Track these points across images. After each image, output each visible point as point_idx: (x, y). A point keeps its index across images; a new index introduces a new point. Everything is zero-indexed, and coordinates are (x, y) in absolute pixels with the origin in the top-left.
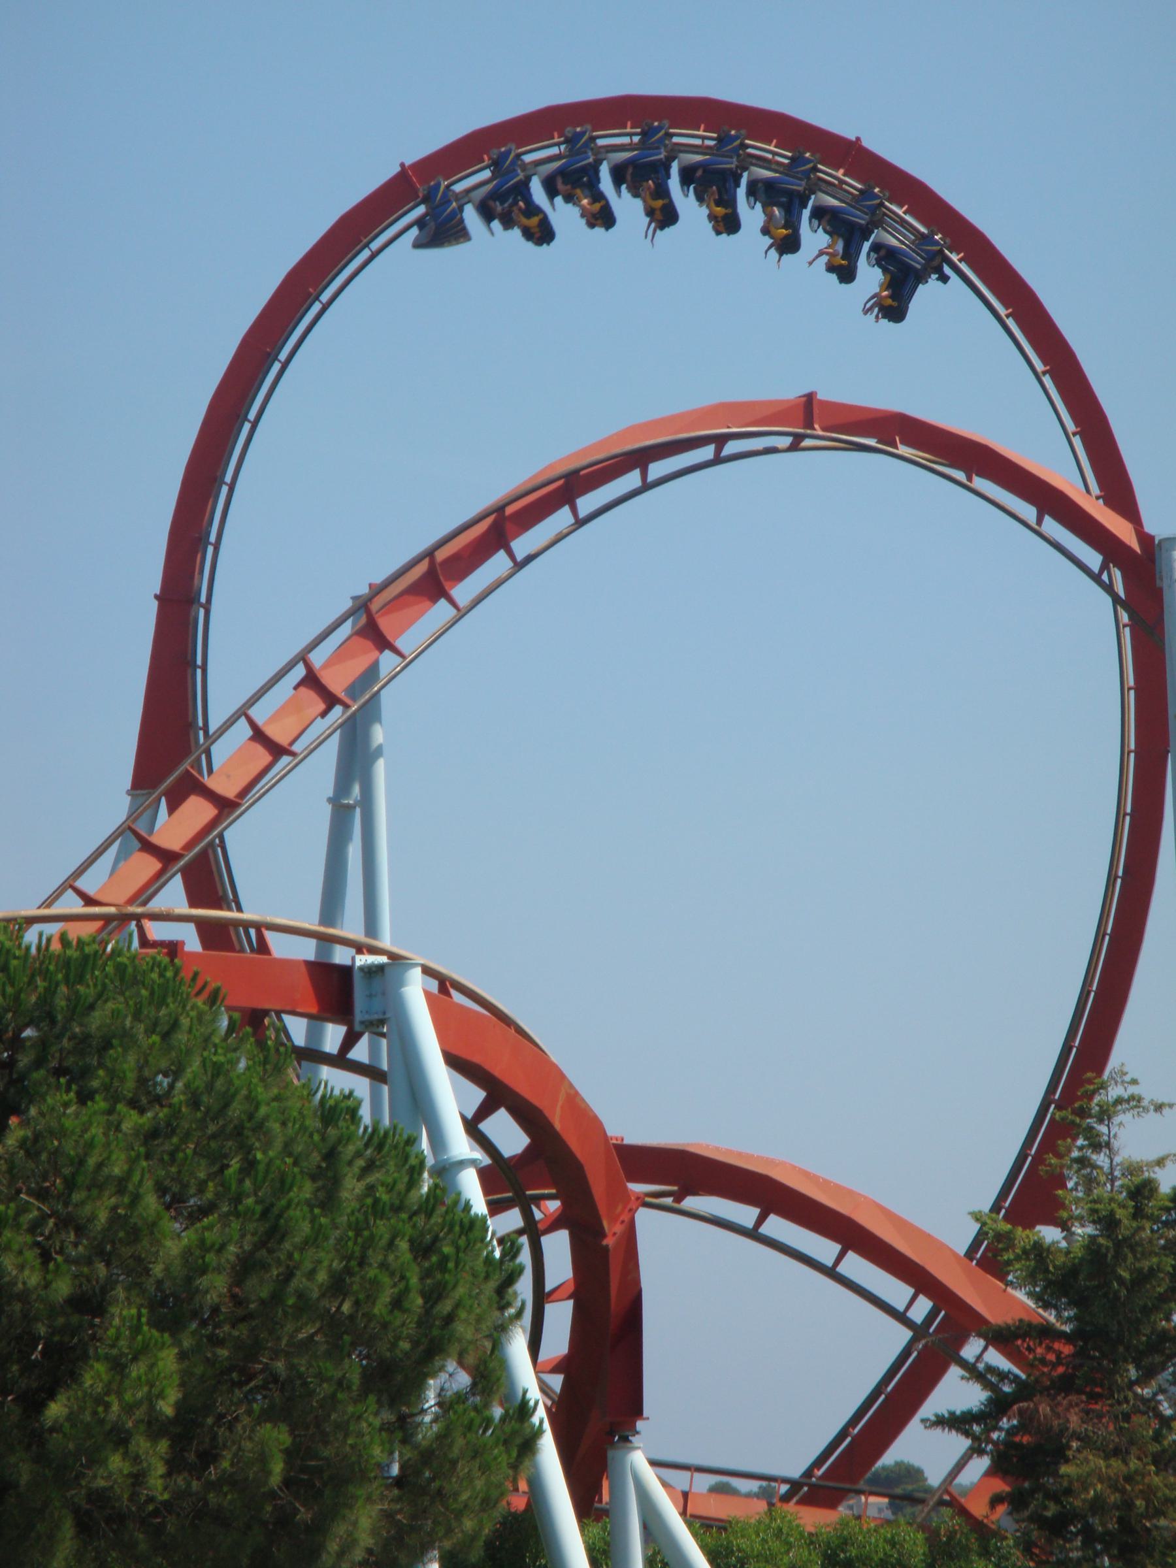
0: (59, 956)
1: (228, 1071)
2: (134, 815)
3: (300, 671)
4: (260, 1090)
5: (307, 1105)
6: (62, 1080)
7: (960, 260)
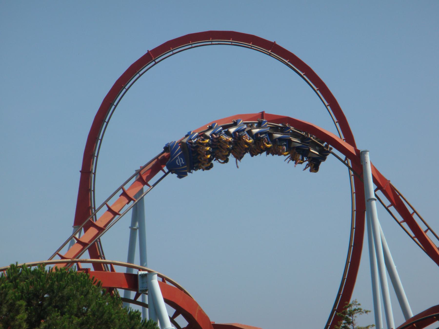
0: (55, 273)
1: (103, 305)
2: (75, 233)
3: (121, 191)
4: (112, 310)
5: (125, 315)
6: (56, 309)
7: (304, 75)
